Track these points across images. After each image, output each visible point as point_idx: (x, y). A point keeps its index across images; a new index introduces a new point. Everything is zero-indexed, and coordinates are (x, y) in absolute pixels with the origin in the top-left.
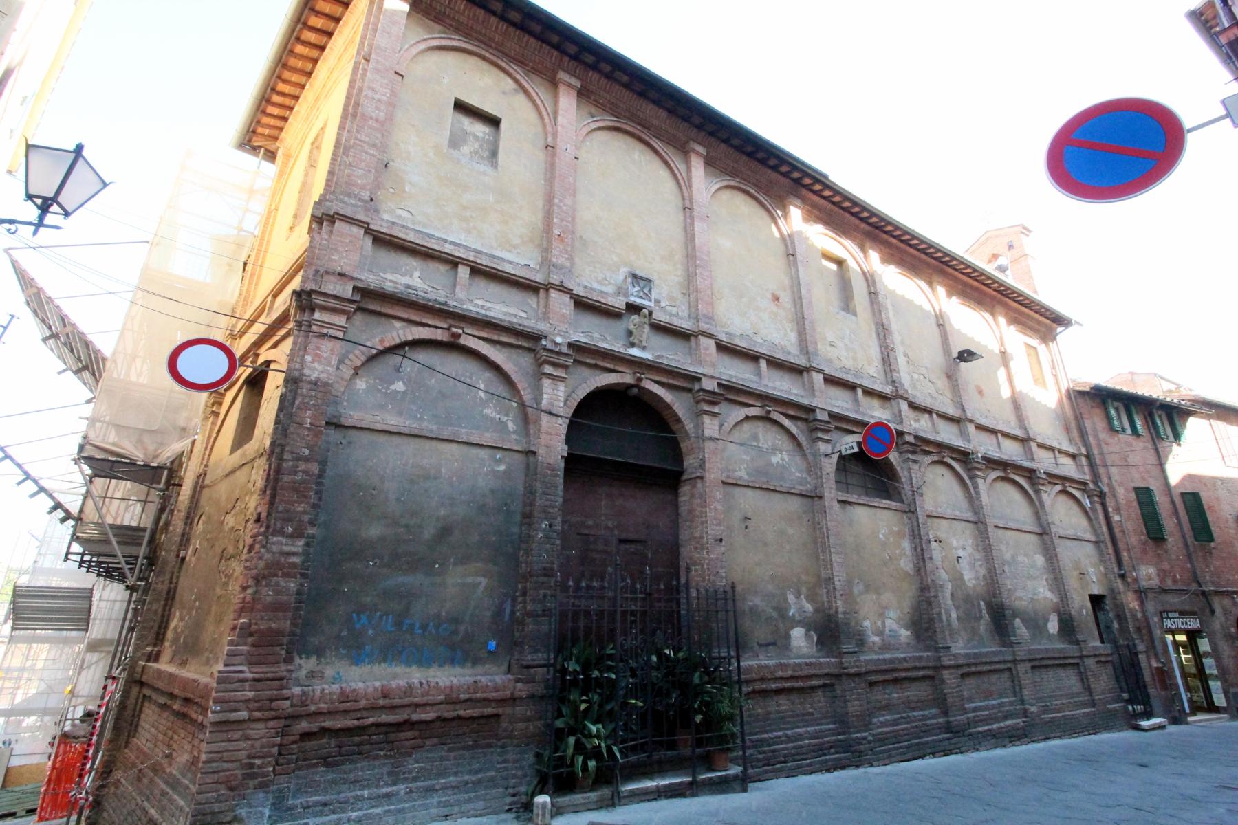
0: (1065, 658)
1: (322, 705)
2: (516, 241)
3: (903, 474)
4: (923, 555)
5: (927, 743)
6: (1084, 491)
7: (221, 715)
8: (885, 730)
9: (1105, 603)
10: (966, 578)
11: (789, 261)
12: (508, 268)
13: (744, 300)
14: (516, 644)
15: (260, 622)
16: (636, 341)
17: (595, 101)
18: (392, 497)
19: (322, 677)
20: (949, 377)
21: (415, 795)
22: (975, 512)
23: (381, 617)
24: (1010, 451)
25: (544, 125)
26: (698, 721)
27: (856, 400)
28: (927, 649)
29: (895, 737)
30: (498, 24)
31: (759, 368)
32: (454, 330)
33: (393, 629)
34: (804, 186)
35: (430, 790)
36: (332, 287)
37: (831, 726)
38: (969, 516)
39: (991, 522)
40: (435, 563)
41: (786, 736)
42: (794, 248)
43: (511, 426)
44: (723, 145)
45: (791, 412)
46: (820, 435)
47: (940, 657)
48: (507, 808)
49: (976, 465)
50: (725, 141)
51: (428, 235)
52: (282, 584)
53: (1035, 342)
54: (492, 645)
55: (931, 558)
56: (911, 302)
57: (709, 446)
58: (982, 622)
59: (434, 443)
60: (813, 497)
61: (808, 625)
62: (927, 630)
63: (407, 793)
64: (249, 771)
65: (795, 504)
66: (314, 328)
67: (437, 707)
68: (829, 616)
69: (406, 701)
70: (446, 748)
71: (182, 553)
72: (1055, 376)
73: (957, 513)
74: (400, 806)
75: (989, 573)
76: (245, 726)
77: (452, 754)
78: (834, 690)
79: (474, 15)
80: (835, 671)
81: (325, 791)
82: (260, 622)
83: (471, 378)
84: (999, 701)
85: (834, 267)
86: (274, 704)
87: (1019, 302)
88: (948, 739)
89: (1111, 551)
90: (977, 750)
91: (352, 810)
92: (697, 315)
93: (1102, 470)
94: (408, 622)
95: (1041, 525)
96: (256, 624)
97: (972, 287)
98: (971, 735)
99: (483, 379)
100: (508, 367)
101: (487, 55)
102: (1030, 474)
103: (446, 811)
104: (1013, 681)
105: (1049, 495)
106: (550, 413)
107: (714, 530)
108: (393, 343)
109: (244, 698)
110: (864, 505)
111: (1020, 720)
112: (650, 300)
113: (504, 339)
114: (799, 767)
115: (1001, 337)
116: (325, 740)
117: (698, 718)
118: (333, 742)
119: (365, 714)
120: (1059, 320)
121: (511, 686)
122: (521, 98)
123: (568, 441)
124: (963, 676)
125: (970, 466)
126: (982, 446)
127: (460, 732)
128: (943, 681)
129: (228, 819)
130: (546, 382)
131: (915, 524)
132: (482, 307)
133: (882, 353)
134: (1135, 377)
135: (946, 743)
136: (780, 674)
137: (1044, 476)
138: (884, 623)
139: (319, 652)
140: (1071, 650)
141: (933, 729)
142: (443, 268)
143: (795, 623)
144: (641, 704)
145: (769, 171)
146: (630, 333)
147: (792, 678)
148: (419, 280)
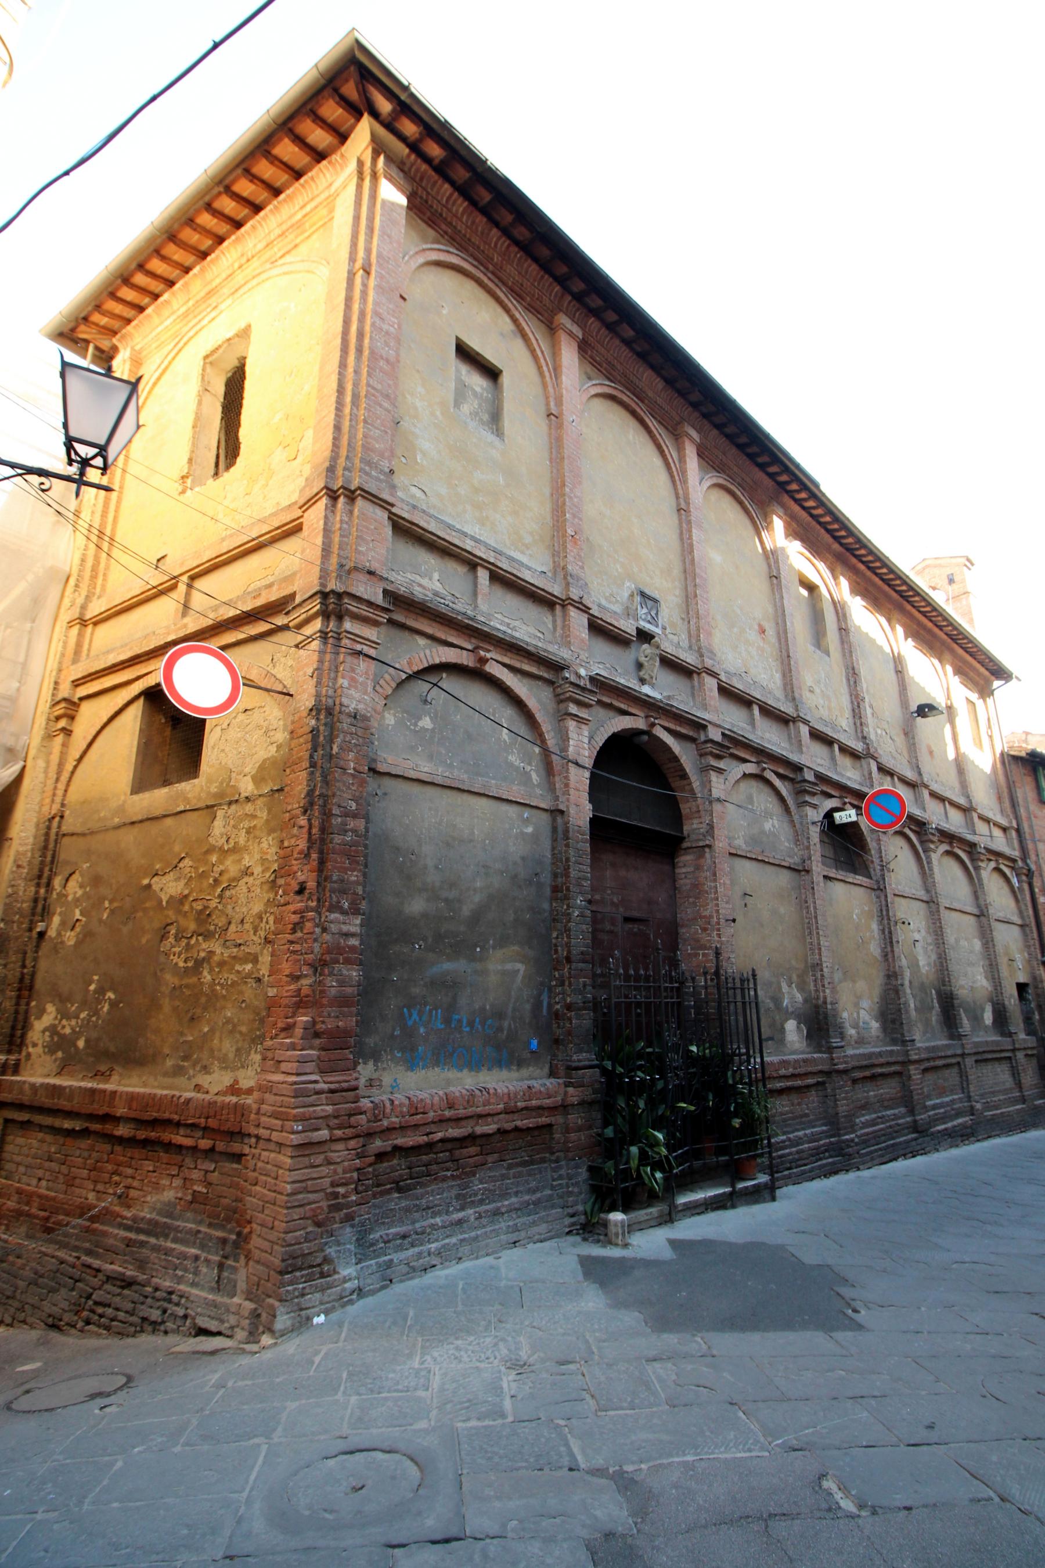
0: (1002, 1051)
1: (394, 1119)
2: (528, 539)
3: (872, 845)
4: (891, 938)
5: (900, 1143)
6: (1013, 868)
7: (303, 1135)
8: (866, 1130)
9: (1027, 992)
10: (921, 963)
11: (772, 584)
12: (527, 576)
13: (735, 630)
14: (557, 1041)
15: (326, 1020)
16: (646, 677)
17: (591, 357)
18: (430, 863)
19: (381, 1086)
20: (906, 734)
21: (484, 1221)
22: (928, 891)
23: (430, 1011)
24: (955, 822)
25: (545, 385)
26: (737, 1126)
27: (833, 759)
28: (894, 1041)
29: (874, 1138)
30: (498, 239)
31: (752, 715)
32: (482, 653)
33: (443, 1026)
34: (788, 492)
35: (497, 1213)
36: (362, 589)
37: (824, 1128)
38: (921, 894)
39: (944, 902)
40: (476, 946)
41: (789, 1139)
42: (778, 570)
43: (534, 776)
44: (715, 432)
45: (781, 771)
46: (808, 798)
47: (908, 1051)
48: (567, 1230)
49: (931, 837)
50: (719, 427)
51: (450, 527)
52: (345, 972)
53: (974, 696)
54: (534, 1043)
55: (898, 942)
56: (873, 642)
57: (717, 807)
58: (934, 1012)
59: (465, 796)
60: (800, 870)
61: (801, 1018)
62: (893, 1021)
63: (476, 1219)
64: (333, 1202)
65: (784, 878)
66: (345, 642)
67: (496, 1118)
68: (817, 1007)
69: (471, 1111)
70: (505, 1164)
71: (40, 927)
72: (991, 737)
73: (914, 892)
74: (473, 1234)
75: (940, 958)
76: (326, 1147)
77: (512, 1172)
78: (826, 1089)
79: (473, 222)
80: (825, 1068)
81: (401, 1221)
82: (326, 1020)
83: (494, 715)
84: (951, 1098)
85: (805, 593)
86: (353, 1120)
87: (965, 649)
88: (915, 1139)
89: (1035, 935)
90: (938, 1151)
91: (429, 1242)
92: (699, 648)
93: (1030, 846)
94: (457, 1017)
95: (978, 906)
96: (323, 1022)
97: (925, 628)
98: (932, 1134)
99: (506, 714)
100: (532, 703)
101: (486, 280)
102: (971, 847)
103: (514, 1237)
104: (961, 1077)
105: (987, 871)
106: (577, 764)
107: (725, 910)
108: (421, 667)
109: (323, 1114)
110: (841, 880)
111: (967, 1119)
112: (657, 626)
113: (527, 667)
114: (804, 1173)
115: (948, 689)
116: (395, 1161)
117: (736, 1122)
118: (404, 1164)
119: (433, 1128)
120: (1000, 672)
121: (562, 1090)
122: (519, 343)
123: (592, 799)
124: (926, 1070)
125: (925, 838)
126: (934, 815)
127: (517, 1146)
128: (910, 1077)
129: (319, 1261)
130: (571, 724)
131: (884, 903)
132: (508, 625)
133: (852, 702)
134: (1030, 737)
135: (914, 1143)
136: (783, 1072)
137: (983, 851)
138: (858, 1013)
139: (375, 1056)
140: (1006, 1043)
141: (903, 1129)
142: (461, 570)
143: (788, 1015)
144: (692, 1108)
145: (756, 469)
146: (640, 666)
147: (794, 1076)
148: (438, 584)
